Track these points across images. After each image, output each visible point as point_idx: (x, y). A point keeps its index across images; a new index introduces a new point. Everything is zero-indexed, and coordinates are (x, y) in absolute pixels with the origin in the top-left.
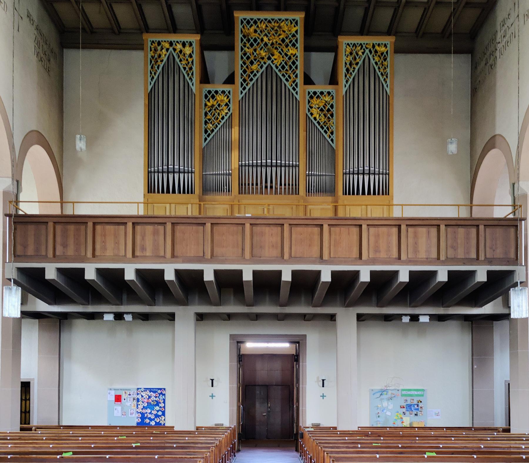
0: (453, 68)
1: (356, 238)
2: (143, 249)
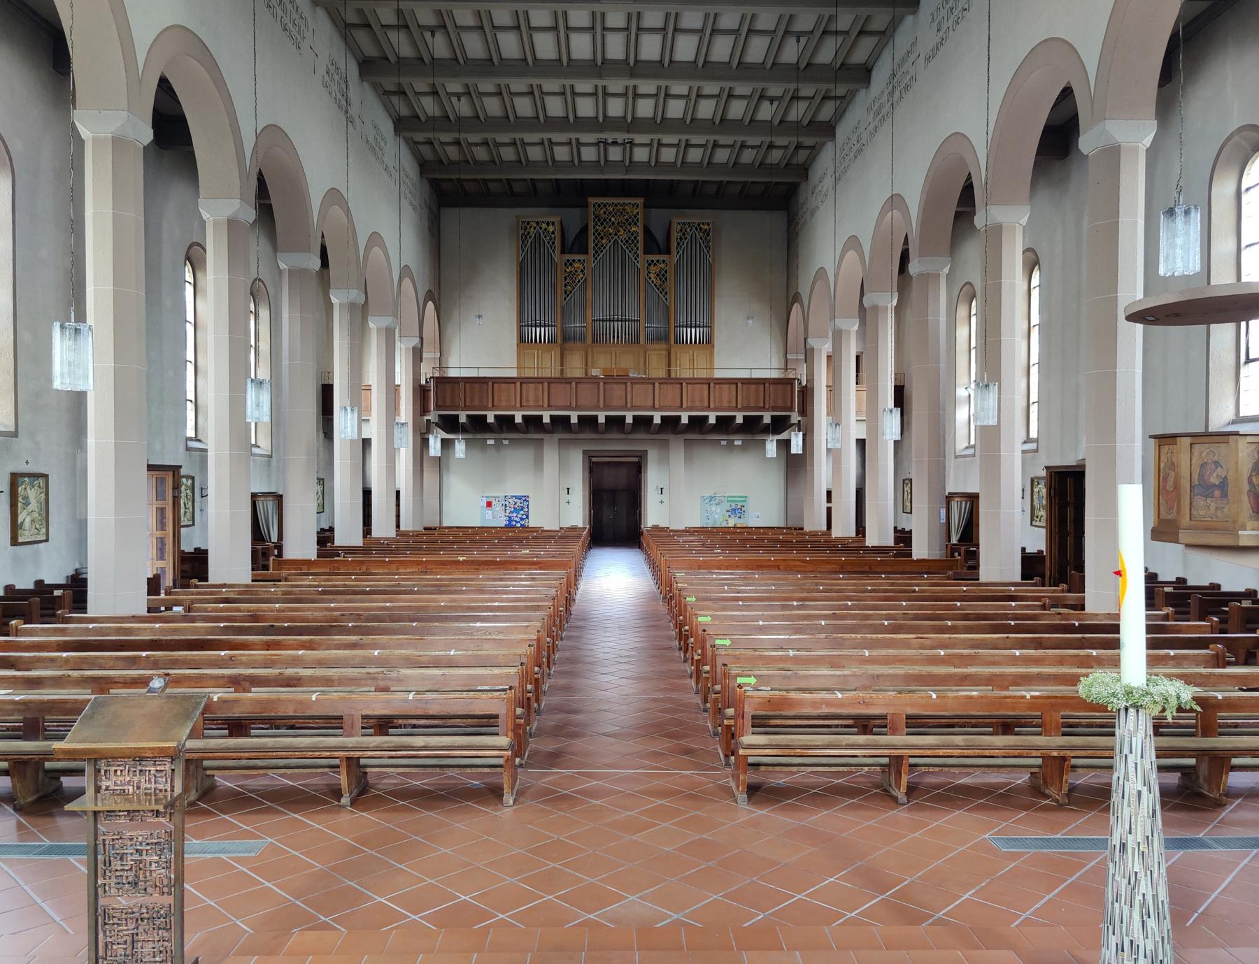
0: (771, 222)
1: (678, 391)
2: (528, 401)
